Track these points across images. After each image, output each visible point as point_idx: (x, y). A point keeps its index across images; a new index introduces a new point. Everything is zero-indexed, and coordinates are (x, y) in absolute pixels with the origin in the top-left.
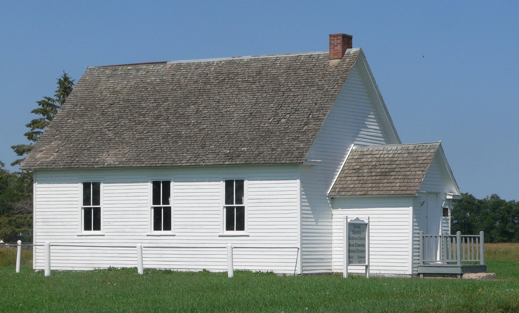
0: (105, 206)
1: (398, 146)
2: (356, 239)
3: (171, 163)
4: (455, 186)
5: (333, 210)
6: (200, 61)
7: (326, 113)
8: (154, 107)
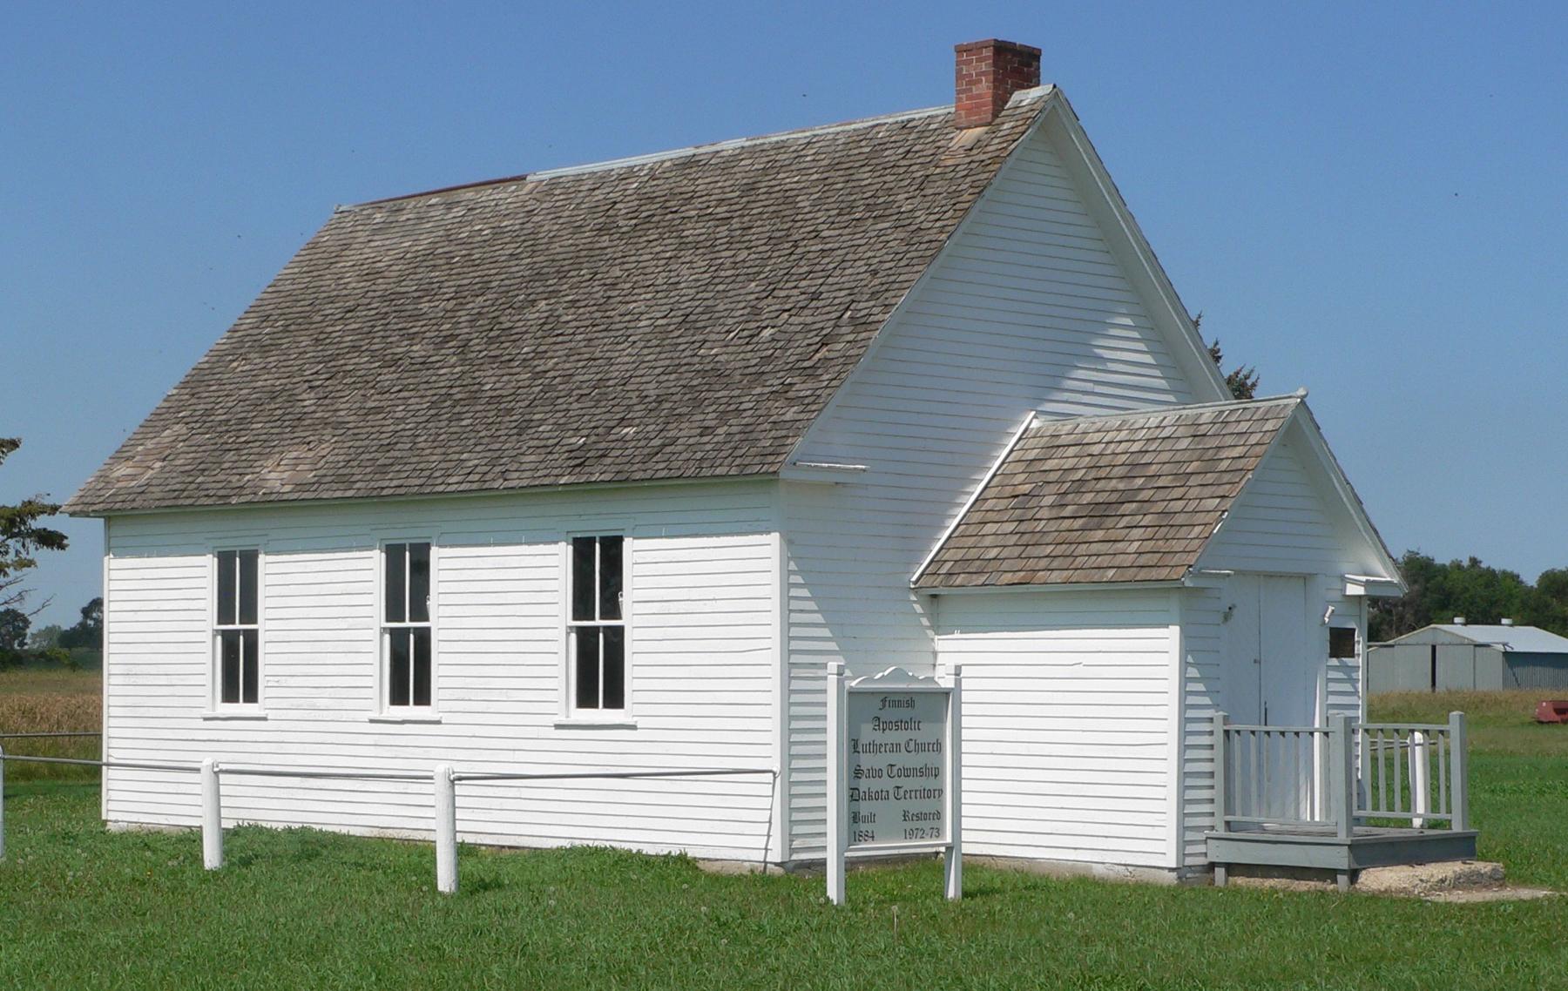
0: (270, 625)
1: (1164, 414)
2: (895, 748)
3: (421, 486)
4: (1376, 547)
5: (936, 637)
6: (610, 167)
7: (893, 301)
8: (447, 311)
